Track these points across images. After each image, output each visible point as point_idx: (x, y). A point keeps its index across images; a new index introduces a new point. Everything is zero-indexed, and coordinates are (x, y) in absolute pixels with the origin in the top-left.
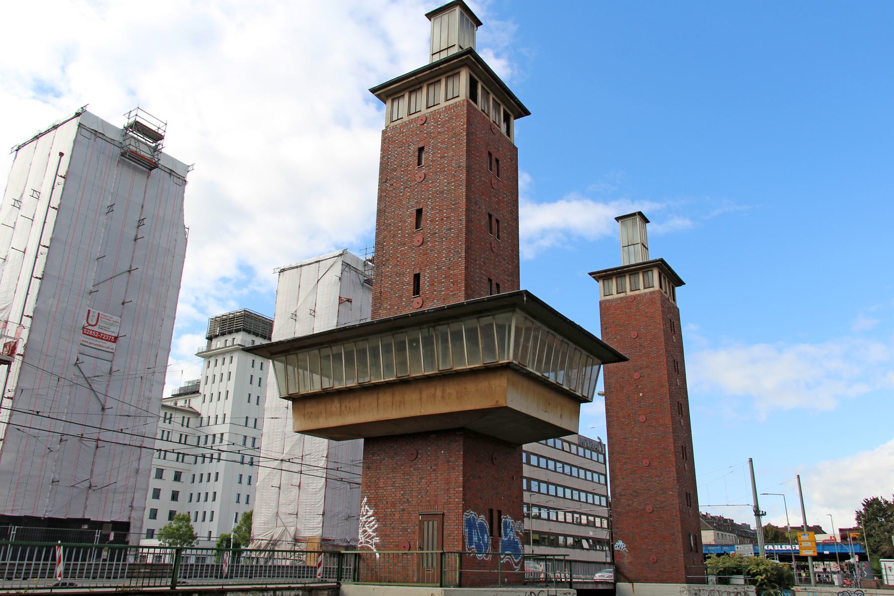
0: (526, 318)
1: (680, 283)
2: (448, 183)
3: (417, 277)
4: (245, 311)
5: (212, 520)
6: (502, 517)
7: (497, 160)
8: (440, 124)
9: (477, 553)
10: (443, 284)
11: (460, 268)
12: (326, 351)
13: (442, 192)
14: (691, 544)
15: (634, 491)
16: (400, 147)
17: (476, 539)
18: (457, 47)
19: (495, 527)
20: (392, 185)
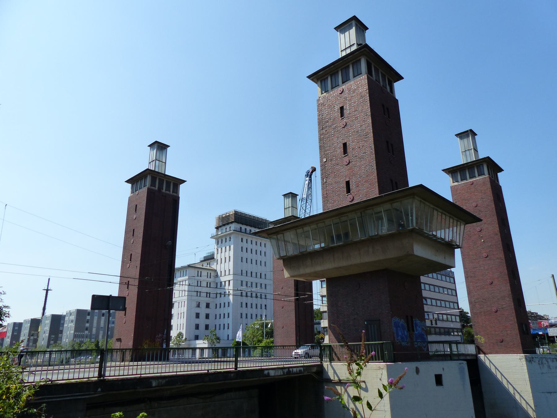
0: (420, 201)
1: (501, 170)
2: (361, 126)
3: (348, 183)
4: (235, 211)
5: (228, 328)
6: (413, 320)
7: (388, 109)
8: (351, 92)
9: (402, 342)
10: (365, 186)
11: (374, 175)
12: (300, 231)
13: (358, 132)
14: (523, 329)
15: (483, 299)
16: (329, 108)
17: (401, 334)
18: (355, 45)
19: (410, 327)
20: (326, 131)
